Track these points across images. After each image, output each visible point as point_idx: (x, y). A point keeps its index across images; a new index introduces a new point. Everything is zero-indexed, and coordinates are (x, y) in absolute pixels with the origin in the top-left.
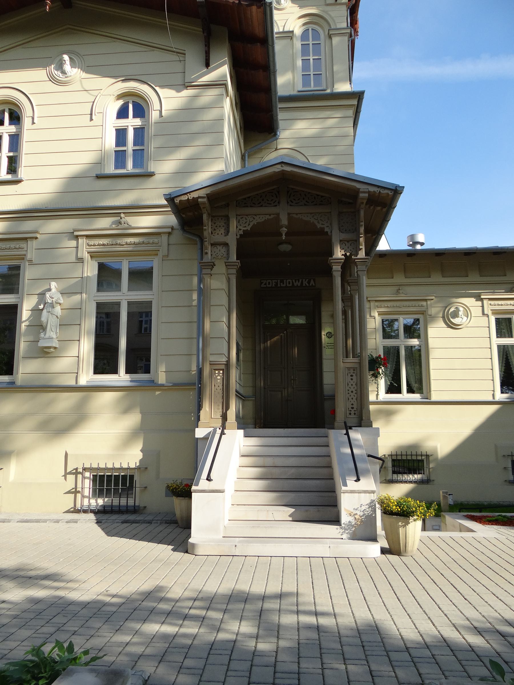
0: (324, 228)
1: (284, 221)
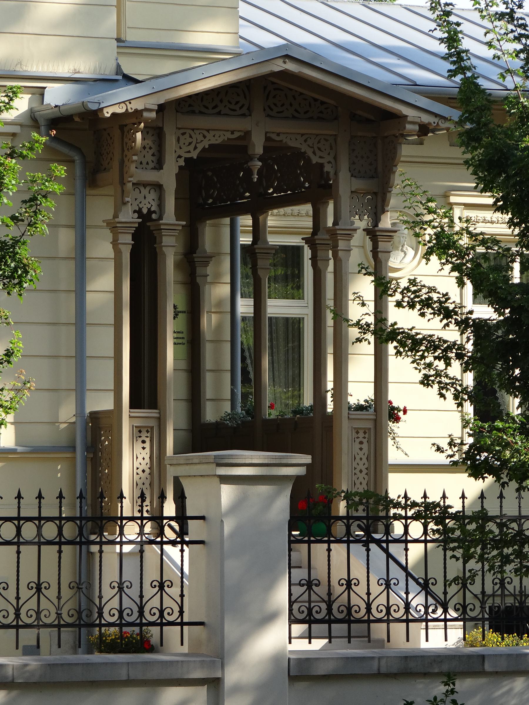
0: (322, 166)
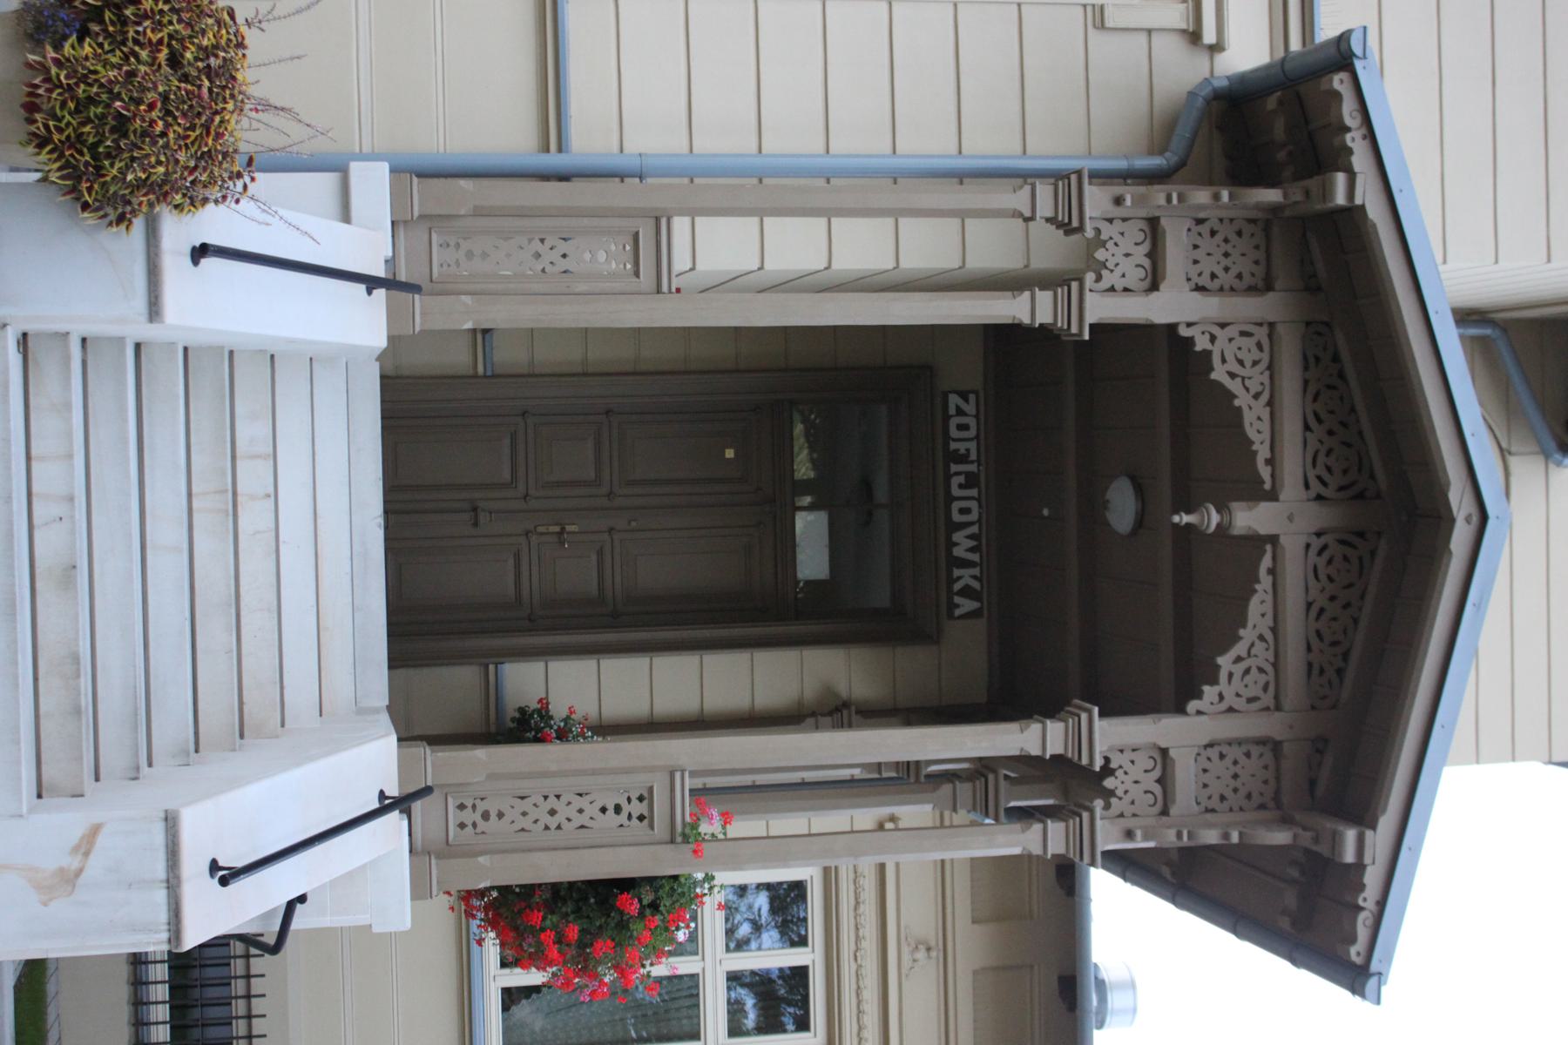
0: (1214, 681)
1: (1248, 518)
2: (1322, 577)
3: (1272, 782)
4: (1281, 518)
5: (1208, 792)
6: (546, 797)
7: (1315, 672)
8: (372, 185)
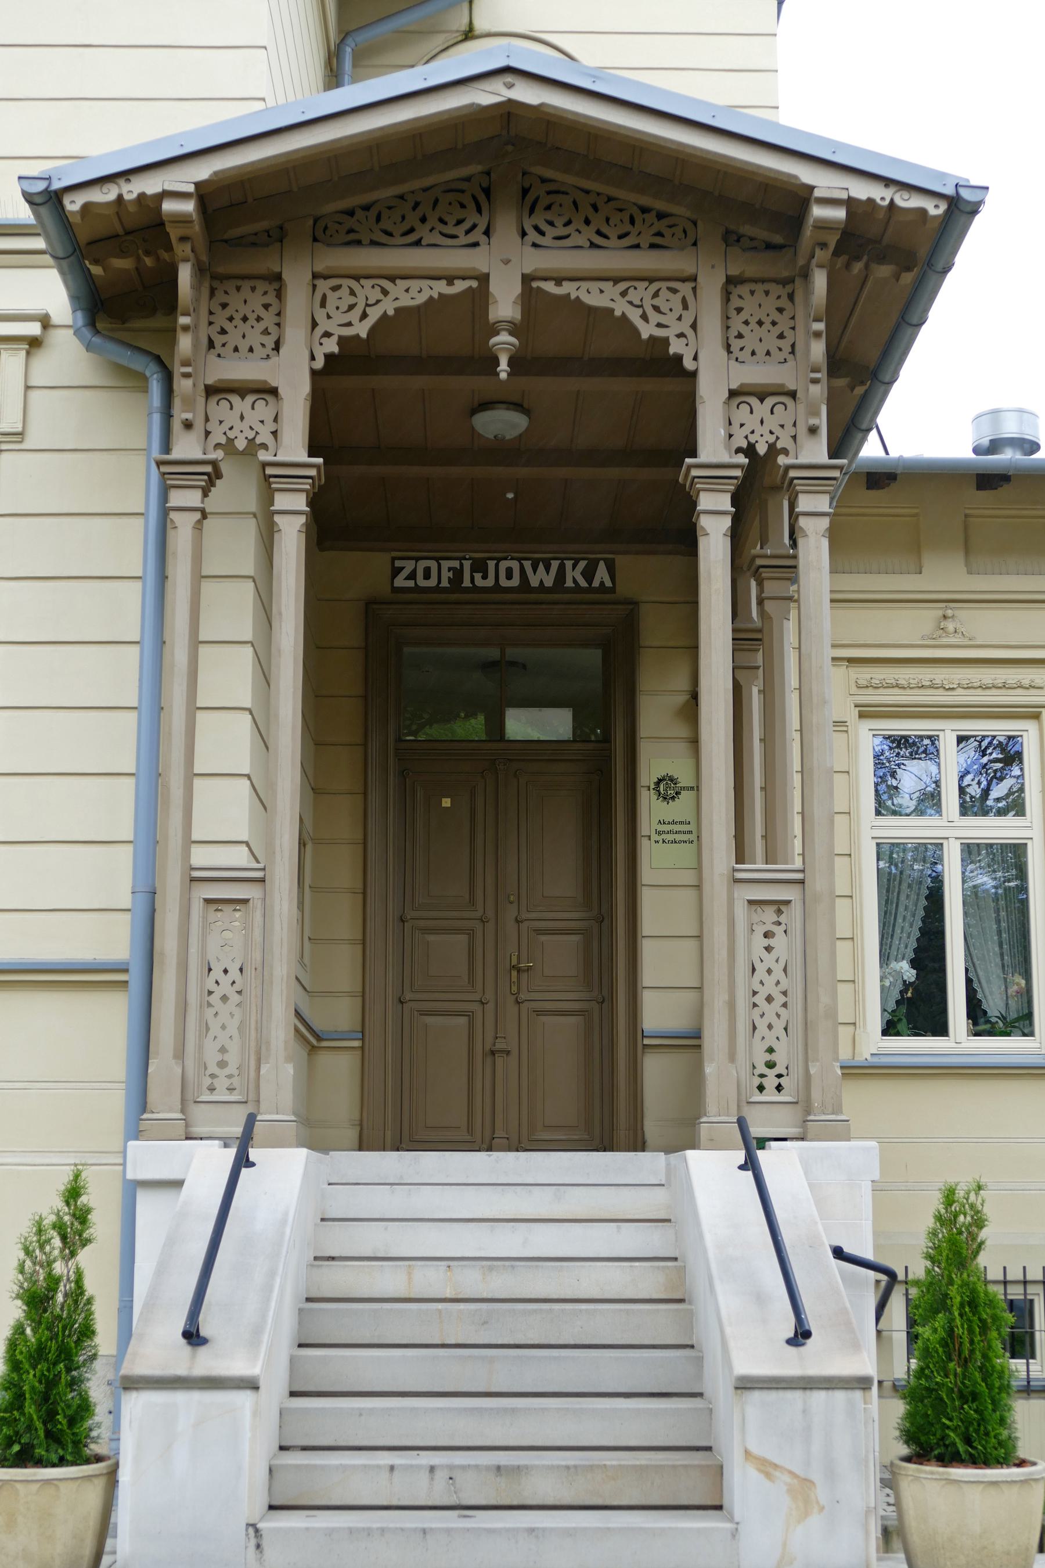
0: (666, 341)
1: (505, 305)
2: (564, 231)
3: (767, 286)
4: (505, 269)
5: (774, 351)
6: (755, 1005)
7: (658, 240)
8: (149, 1158)
